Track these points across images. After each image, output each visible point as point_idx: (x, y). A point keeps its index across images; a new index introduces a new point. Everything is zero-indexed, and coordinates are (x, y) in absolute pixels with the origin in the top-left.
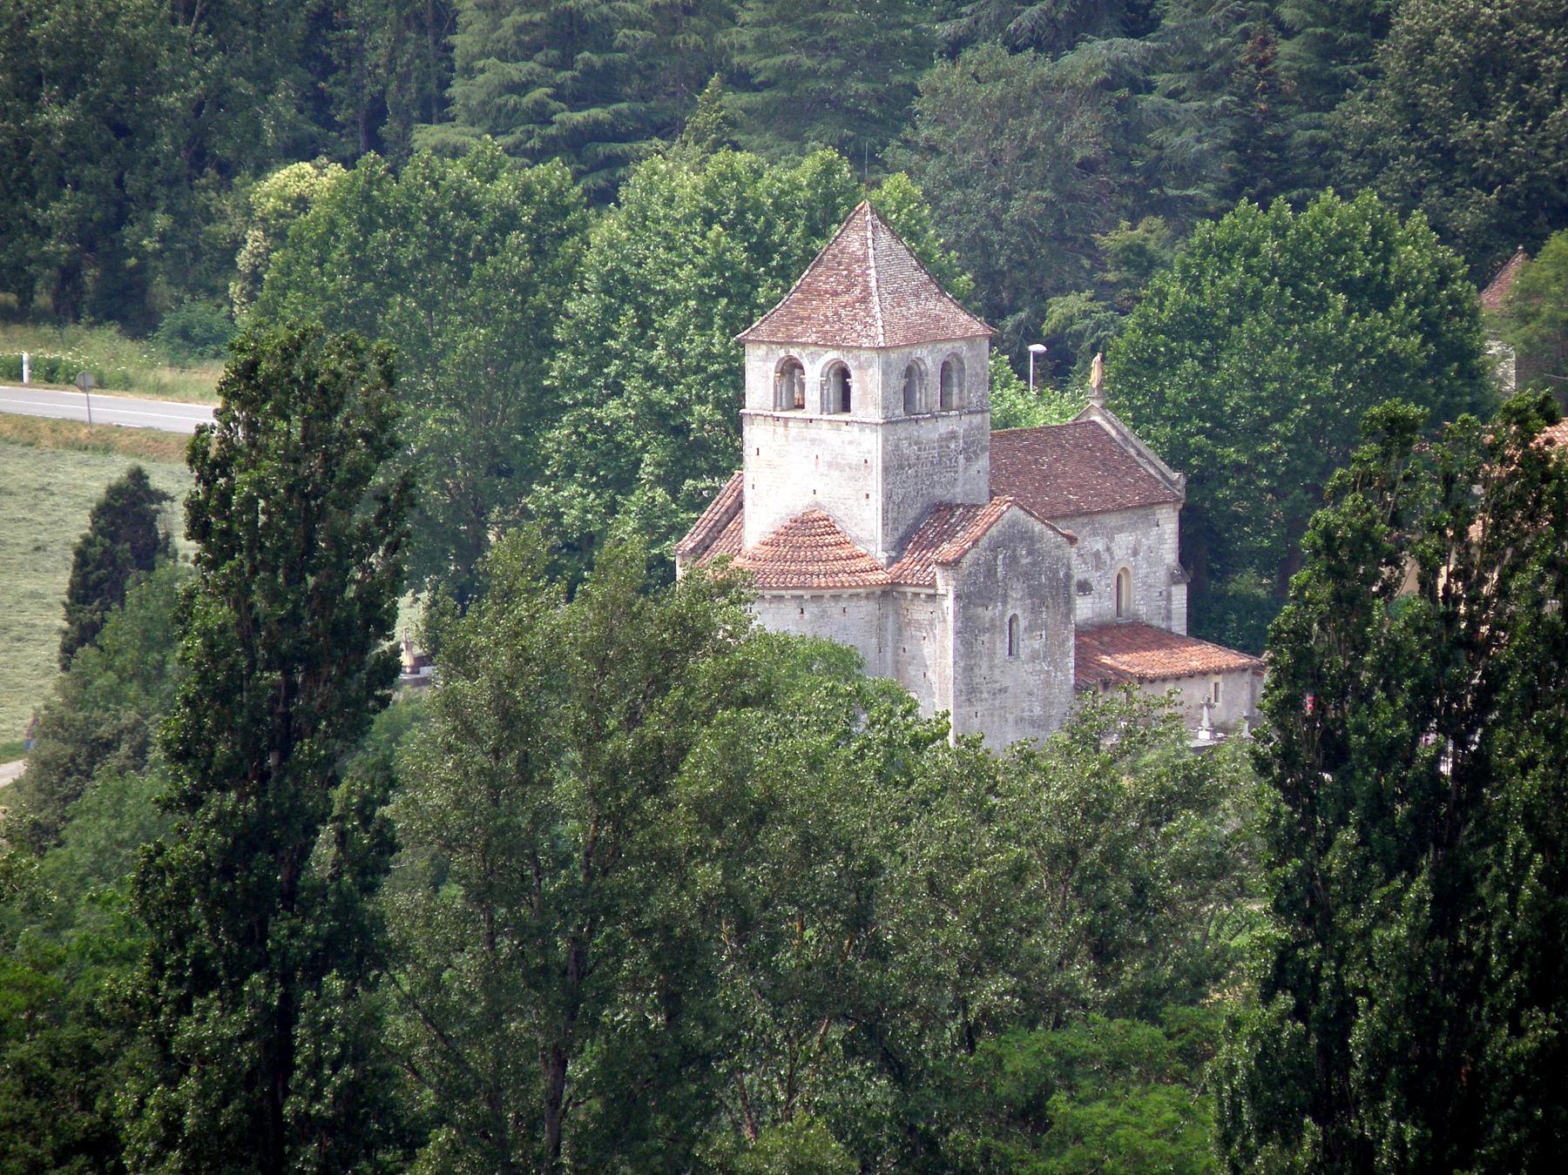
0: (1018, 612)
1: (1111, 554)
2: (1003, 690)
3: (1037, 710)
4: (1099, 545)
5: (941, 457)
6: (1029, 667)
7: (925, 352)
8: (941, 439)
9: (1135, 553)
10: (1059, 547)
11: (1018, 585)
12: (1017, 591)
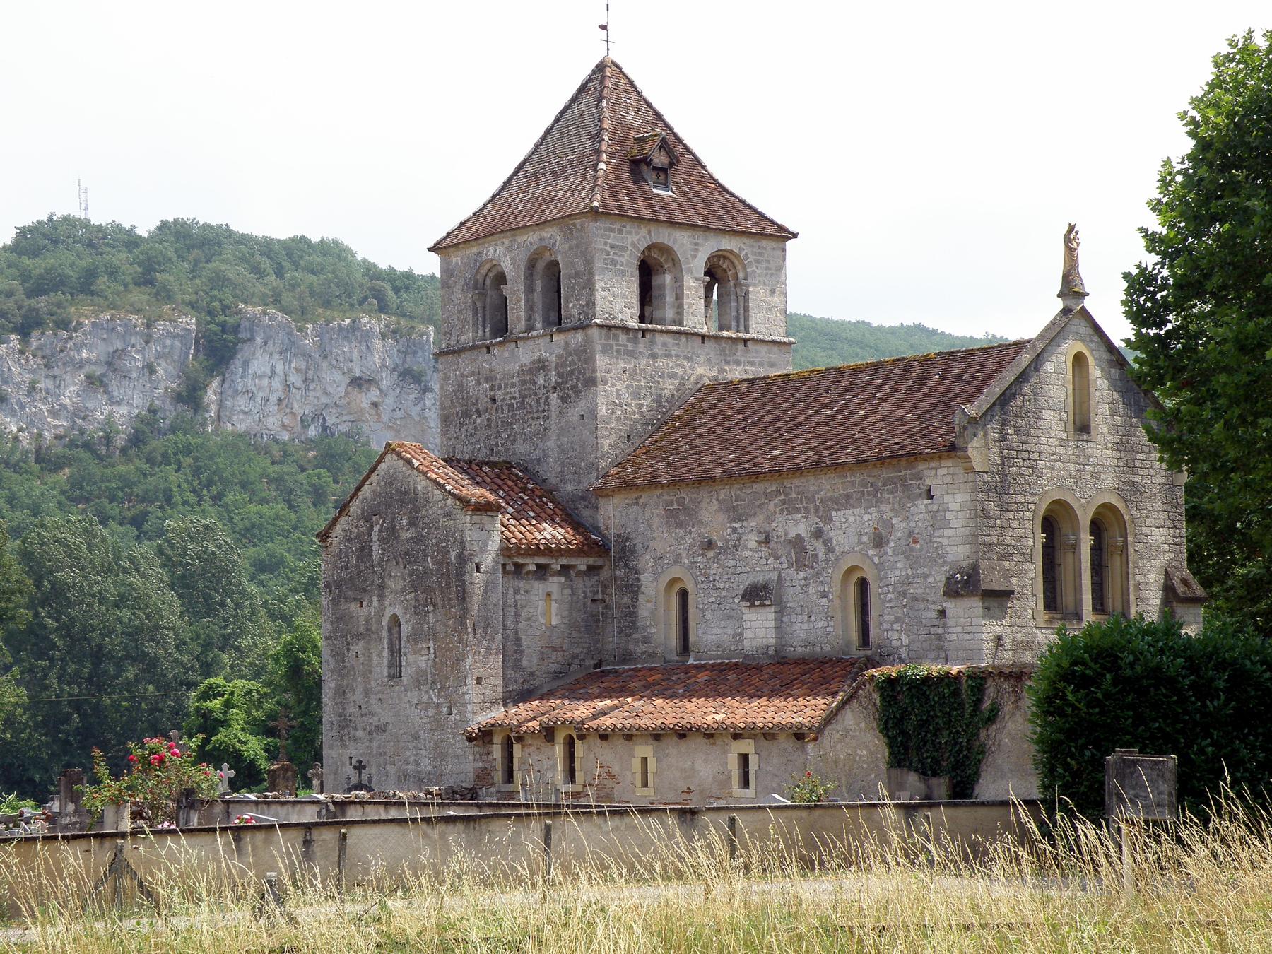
0: (399, 611)
1: (827, 543)
2: (381, 728)
3: (426, 765)
4: (800, 527)
5: (523, 397)
6: (413, 696)
7: (501, 250)
8: (524, 371)
9: (879, 542)
10: (448, 514)
11: (397, 572)
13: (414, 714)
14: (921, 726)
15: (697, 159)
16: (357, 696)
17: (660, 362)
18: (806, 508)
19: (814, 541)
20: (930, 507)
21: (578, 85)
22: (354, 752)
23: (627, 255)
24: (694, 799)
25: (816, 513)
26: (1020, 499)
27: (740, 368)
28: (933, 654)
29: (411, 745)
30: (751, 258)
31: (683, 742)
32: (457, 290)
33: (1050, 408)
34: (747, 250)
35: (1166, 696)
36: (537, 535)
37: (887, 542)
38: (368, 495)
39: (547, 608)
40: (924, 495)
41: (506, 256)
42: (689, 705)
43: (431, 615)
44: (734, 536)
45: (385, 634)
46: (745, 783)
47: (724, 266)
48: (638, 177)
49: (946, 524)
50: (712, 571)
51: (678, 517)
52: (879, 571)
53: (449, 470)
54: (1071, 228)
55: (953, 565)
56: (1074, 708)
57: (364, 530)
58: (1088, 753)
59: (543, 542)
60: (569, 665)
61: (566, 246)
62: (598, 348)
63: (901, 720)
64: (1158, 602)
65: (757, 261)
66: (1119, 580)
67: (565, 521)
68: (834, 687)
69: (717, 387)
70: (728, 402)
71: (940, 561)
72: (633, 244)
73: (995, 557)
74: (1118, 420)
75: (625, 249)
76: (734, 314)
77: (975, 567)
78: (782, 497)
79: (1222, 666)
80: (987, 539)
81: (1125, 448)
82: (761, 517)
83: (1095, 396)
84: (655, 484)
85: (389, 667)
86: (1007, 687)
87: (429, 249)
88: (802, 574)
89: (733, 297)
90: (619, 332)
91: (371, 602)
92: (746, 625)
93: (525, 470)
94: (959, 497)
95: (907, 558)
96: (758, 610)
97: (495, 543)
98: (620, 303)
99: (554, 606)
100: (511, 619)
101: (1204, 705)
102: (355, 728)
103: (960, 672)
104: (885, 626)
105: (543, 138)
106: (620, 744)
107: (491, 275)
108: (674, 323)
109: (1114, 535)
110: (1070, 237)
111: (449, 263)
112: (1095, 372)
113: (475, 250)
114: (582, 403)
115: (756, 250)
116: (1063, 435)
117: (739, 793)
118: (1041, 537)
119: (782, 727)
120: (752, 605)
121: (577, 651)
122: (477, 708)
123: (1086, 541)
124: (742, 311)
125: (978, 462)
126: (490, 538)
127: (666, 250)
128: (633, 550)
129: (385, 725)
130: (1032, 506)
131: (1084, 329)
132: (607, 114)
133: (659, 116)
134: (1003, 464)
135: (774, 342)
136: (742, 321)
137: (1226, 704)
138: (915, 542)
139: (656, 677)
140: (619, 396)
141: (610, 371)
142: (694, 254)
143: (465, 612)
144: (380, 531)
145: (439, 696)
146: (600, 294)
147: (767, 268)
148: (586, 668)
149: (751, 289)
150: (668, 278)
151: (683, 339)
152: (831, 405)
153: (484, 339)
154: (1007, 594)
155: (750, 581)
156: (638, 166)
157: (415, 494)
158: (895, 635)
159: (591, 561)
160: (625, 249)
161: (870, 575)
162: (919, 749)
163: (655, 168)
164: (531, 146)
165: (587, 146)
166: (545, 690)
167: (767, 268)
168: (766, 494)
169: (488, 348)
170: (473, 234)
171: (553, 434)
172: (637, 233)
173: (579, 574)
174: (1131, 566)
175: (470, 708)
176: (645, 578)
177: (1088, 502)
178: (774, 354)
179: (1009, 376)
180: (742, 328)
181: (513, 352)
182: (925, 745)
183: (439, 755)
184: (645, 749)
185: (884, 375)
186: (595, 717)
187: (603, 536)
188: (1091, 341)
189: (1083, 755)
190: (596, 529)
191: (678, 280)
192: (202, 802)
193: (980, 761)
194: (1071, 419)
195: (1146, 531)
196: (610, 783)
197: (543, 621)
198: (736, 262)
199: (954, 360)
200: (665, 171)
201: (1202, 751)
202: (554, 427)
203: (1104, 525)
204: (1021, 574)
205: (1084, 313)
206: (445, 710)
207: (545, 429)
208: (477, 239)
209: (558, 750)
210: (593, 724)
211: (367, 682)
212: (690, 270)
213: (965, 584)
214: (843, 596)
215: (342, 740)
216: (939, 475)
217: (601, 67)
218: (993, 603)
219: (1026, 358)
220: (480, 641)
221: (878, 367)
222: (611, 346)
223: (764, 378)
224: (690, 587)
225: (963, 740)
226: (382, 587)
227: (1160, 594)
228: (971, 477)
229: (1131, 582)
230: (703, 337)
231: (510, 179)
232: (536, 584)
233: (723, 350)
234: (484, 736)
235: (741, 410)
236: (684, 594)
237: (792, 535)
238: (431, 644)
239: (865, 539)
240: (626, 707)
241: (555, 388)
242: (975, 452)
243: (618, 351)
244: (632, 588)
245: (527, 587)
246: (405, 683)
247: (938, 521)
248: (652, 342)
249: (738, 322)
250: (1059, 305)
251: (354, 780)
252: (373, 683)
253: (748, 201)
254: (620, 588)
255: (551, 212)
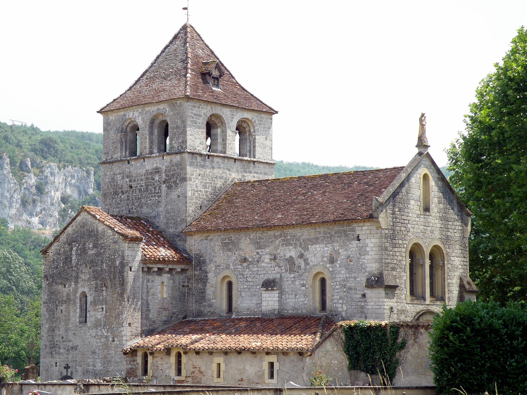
0: (86, 290)
1: (306, 261)
2: (74, 348)
3: (99, 366)
4: (292, 252)
5: (147, 186)
6: (93, 332)
9: (332, 261)
10: (115, 242)
11: (86, 270)
12: (85, 274)
13: (94, 341)
14: (366, 350)
15: (231, 74)
16: (61, 332)
17: (216, 171)
18: (295, 244)
19: (299, 260)
20: (359, 245)
21: (173, 35)
22: (58, 360)
23: (201, 118)
24: (244, 384)
25: (300, 246)
26: (400, 242)
27: (251, 175)
28: (359, 315)
29: (91, 357)
30: (257, 122)
31: (198, 356)
32: (112, 133)
33: (413, 199)
34: (255, 118)
35: (494, 338)
36: (158, 253)
37: (337, 261)
38: (70, 232)
39: (162, 289)
40: (356, 239)
41: (139, 117)
42: (240, 338)
43: (104, 292)
44: (258, 256)
45: (78, 301)
46: (272, 376)
47: (244, 126)
48: (205, 82)
49: (367, 253)
50: (246, 273)
51: (227, 246)
52: (332, 275)
53: (114, 220)
54: (423, 115)
55: (370, 272)
56: (454, 343)
57: (68, 249)
58: (459, 365)
59: (162, 257)
60: (171, 317)
61: (172, 113)
62: (188, 163)
63: (355, 347)
64: (457, 292)
65: (260, 124)
66: (440, 281)
67: (171, 247)
68: (313, 330)
69: (242, 184)
70: (249, 191)
71: (363, 271)
72: (204, 114)
73: (390, 269)
74: (441, 206)
75: (200, 116)
76: (248, 149)
77: (381, 274)
78: (283, 238)
79: (519, 324)
80: (387, 261)
81: (444, 219)
82: (272, 247)
83: (432, 194)
84: (218, 230)
85: (80, 317)
86: (410, 332)
87: (98, 112)
88: (292, 275)
89: (248, 141)
90: (198, 156)
91: (71, 285)
92: (263, 299)
93: (147, 221)
94: (373, 240)
95: (347, 269)
96: (270, 292)
97: (139, 258)
98: (198, 142)
99: (165, 288)
100: (145, 294)
101: (512, 343)
102: (59, 348)
103: (386, 324)
104: (335, 301)
105: (156, 60)
106: (206, 357)
107: (130, 126)
108: (221, 152)
109: (438, 258)
110: (422, 119)
111: (108, 119)
112: (432, 183)
113: (122, 113)
114: (179, 190)
115: (259, 118)
116: (419, 212)
117: (268, 381)
118: (409, 260)
119: (293, 349)
120: (267, 290)
121: (175, 311)
122: (128, 338)
123: (428, 262)
124: (252, 148)
125: (383, 225)
126: (136, 255)
127: (218, 117)
128: (204, 262)
129: (77, 346)
130: (405, 246)
131: (428, 163)
132: (189, 50)
133: (212, 52)
134: (393, 225)
135: (267, 163)
136: (252, 152)
137: (521, 343)
138: (351, 261)
139: (218, 324)
140: (197, 187)
141: (193, 175)
142: (231, 118)
143: (123, 291)
144: (77, 250)
145: (107, 332)
146: (189, 137)
147: (264, 128)
148: (179, 319)
149: (257, 137)
150: (219, 130)
151: (226, 160)
152: (304, 195)
153: (125, 157)
154: (395, 287)
155: (266, 278)
156: (205, 76)
157: (97, 232)
158: (340, 306)
159: (183, 266)
160: (200, 116)
161: (327, 277)
162: (365, 361)
163: (213, 78)
164: (149, 64)
165: (180, 65)
166: (160, 329)
167: (264, 128)
168: (275, 236)
169: (128, 161)
170: (121, 105)
171: (163, 205)
172: (206, 109)
173: (177, 273)
174: (446, 275)
175: (124, 338)
176: (210, 275)
177: (429, 244)
178: (267, 169)
179: (396, 183)
180: (252, 156)
181: (142, 163)
182: (368, 359)
183: (106, 361)
184: (219, 359)
185: (329, 181)
186: (192, 343)
187: (188, 254)
188: (431, 168)
189: (457, 366)
190: (185, 251)
191: (224, 132)
192: (8, 384)
193: (396, 367)
194: (422, 205)
195: (453, 258)
196: (200, 376)
197: (159, 296)
198: (250, 124)
199: (364, 175)
200: (217, 79)
201: (511, 365)
202: (163, 201)
203: (436, 254)
204: (400, 277)
205: (428, 155)
206: (111, 339)
207: (159, 202)
208: (124, 108)
209: (173, 359)
210: (192, 346)
211: (67, 325)
212: (229, 127)
213: (376, 282)
214: (313, 287)
215: (51, 353)
216: (363, 230)
217: (185, 27)
218: (389, 292)
219: (403, 176)
220: (131, 305)
221: (325, 177)
222: (194, 162)
223: (266, 180)
224: (234, 280)
225: (388, 357)
226: (77, 277)
227: (458, 289)
228: (379, 231)
229: (446, 283)
230: (235, 159)
231: (139, 80)
232: (157, 277)
233: (244, 166)
234: (133, 352)
235: (256, 195)
236: (230, 284)
237: (288, 256)
238: (104, 306)
239: (325, 259)
240: (207, 339)
241: (164, 182)
242: (382, 219)
243: (197, 165)
244: (204, 280)
245: (153, 279)
246: (89, 325)
247: (362, 251)
248: (213, 161)
249: (250, 153)
250: (416, 151)
251: (64, 373)
252: (70, 326)
253: (255, 95)
254: (197, 280)
255: (164, 96)
